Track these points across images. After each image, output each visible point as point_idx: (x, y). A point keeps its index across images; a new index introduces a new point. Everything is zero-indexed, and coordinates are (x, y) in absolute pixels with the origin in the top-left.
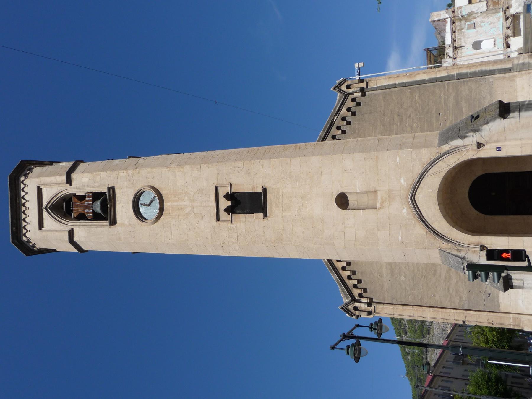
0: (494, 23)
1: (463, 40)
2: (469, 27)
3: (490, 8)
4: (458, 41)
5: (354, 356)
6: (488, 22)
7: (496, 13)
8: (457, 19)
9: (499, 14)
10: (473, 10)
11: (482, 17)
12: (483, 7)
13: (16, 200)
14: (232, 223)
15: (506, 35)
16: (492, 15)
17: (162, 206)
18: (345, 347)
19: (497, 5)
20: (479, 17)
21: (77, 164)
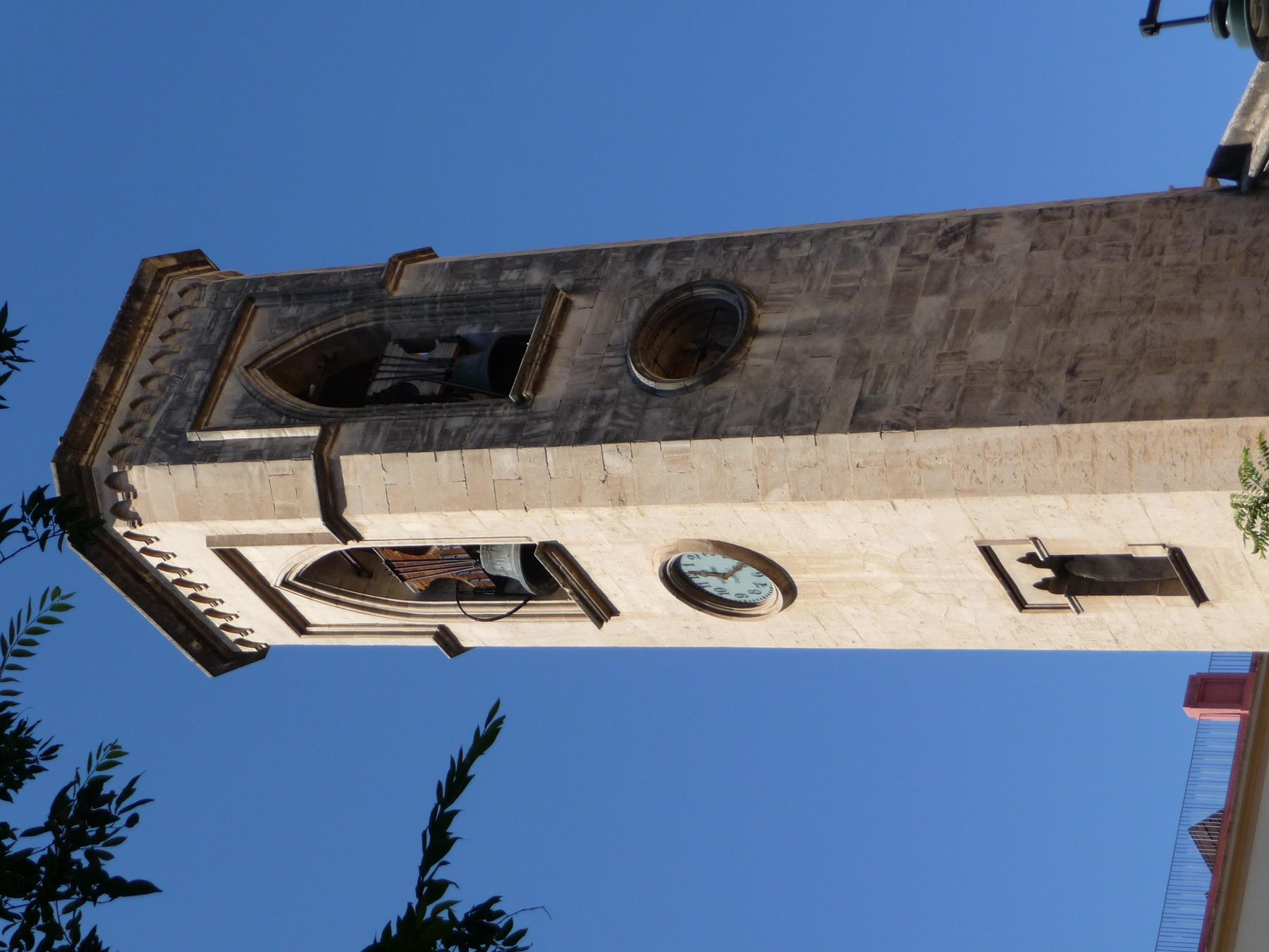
13: (141, 580)
14: (1078, 612)
17: (785, 584)
21: (327, 466)
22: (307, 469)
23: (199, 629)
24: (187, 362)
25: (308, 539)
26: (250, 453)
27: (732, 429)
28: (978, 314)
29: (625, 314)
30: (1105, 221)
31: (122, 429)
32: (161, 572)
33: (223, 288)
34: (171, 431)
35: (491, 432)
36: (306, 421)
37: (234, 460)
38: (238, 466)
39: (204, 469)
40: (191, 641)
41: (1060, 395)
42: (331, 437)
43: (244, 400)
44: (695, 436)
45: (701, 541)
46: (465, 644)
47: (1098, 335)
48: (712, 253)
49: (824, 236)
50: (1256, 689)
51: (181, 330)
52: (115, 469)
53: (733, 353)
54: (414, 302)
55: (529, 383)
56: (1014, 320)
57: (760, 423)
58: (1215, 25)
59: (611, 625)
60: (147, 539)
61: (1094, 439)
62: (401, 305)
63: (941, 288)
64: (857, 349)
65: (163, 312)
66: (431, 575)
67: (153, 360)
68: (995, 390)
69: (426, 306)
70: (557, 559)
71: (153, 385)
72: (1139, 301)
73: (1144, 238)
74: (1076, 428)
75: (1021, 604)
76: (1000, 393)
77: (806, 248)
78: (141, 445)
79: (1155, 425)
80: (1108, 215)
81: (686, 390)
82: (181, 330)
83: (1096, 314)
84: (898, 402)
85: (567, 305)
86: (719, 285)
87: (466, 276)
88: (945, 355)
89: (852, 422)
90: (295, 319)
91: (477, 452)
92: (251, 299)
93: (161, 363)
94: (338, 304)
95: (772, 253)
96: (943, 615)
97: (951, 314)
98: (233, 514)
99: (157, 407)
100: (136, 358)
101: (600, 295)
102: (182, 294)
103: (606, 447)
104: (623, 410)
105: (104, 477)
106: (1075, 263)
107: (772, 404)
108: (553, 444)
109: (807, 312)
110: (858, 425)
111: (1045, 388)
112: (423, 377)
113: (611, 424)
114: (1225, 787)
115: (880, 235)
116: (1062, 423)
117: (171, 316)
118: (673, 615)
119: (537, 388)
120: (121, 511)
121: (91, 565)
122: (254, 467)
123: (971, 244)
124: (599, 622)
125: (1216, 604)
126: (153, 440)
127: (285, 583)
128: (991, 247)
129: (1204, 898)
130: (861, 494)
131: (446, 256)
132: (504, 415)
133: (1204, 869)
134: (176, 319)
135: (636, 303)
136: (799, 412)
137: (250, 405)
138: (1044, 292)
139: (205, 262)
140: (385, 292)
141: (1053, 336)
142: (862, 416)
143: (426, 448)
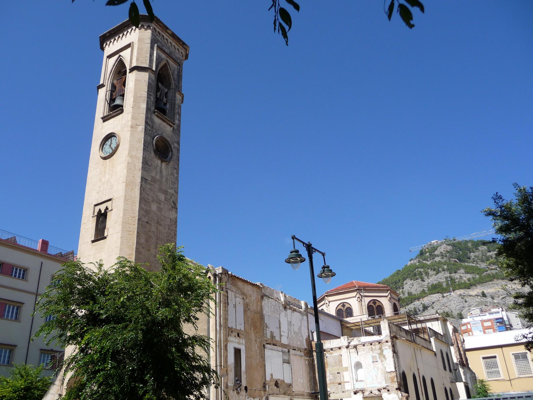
1: (363, 352)
2: (373, 357)
3: (389, 375)
4: (363, 348)
6: (377, 374)
7: (386, 380)
8: (381, 346)
9: (385, 383)
10: (387, 360)
11: (382, 368)
13: (125, 27)
15: (364, 391)
16: (384, 377)
18: (296, 248)
20: (382, 366)
22: (147, 65)
23: (111, 36)
24: (169, 49)
25: (131, 62)
26: (151, 55)
27: (144, 153)
28: (160, 206)
29: (168, 137)
31: (159, 32)
32: (127, 31)
33: (181, 61)
34: (157, 41)
35: (150, 104)
36: (156, 68)
37: (150, 52)
38: (149, 52)
39: (149, 45)
40: (109, 34)
41: (143, 219)
42: (152, 72)
45: (120, 142)
47: (153, 229)
48: (177, 157)
50: (44, 254)
51: (175, 50)
52: (151, 28)
53: (159, 156)
54: (175, 97)
55: (158, 115)
56: (158, 213)
58: (294, 250)
59: (101, 121)
61: (134, 225)
62: (175, 94)
63: (165, 200)
64: (156, 181)
66: (117, 86)
67: (170, 42)
68: (146, 207)
69: (174, 99)
70: (119, 112)
71: (166, 41)
72: (159, 238)
73: (170, 240)
75: (96, 205)
76: (145, 208)
78: (155, 35)
79: (135, 237)
80: (175, 234)
81: (153, 145)
82: (175, 50)
83: (157, 229)
84: (146, 187)
85: (171, 126)
86: (171, 157)
87: (178, 108)
88: (153, 198)
89: (143, 177)
91: (146, 100)
92: (179, 65)
94: (176, 81)
95: (175, 169)
96: (95, 189)
98: (139, 49)
101: (172, 133)
102: (181, 52)
104: (151, 132)
105: (150, 25)
108: (146, 116)
109: (164, 173)
110: (142, 178)
111: (145, 216)
112: (160, 94)
113: (148, 129)
114: (24, 245)
115: (176, 190)
116: (138, 219)
117: (178, 49)
119: (157, 116)
121: (115, 27)
122: (148, 55)
124: (102, 118)
125: (91, 245)
126: (156, 37)
128: (172, 211)
130: (127, 176)
131: (182, 105)
132: (152, 108)
134: (177, 50)
135: (170, 140)
136: (146, 167)
137: (160, 59)
138: (162, 219)
140: (178, 91)
141: (154, 220)
142: (144, 179)
143: (148, 90)
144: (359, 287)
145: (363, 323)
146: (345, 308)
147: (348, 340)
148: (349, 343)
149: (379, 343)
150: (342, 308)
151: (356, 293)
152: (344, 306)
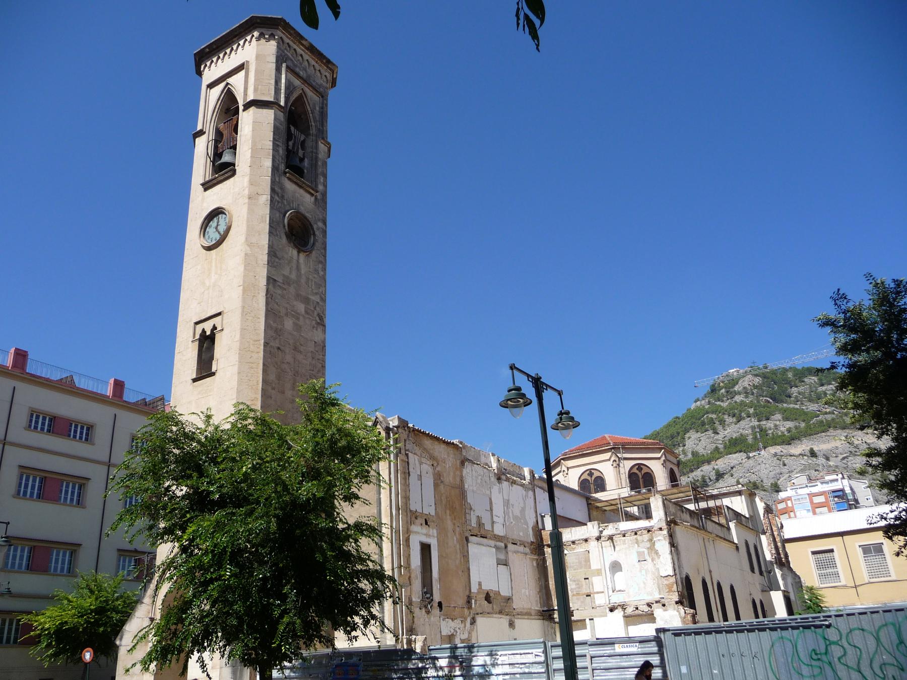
0: (645, 588)
1: (623, 546)
2: (639, 554)
5: (508, 400)
6: (646, 580)
12: (666, 570)
13: (235, 37)
16: (656, 585)
17: (212, 248)
19: (668, 590)
22: (270, 98)
24: (306, 71)
28: (298, 322)
30: (321, 365)
31: (288, 44)
35: (277, 161)
36: (286, 102)
39: (274, 66)
43: (293, 85)
44: (270, 226)
46: (197, 139)
47: (289, 358)
49: (324, 278)
52: (276, 37)
53: (294, 243)
54: (317, 147)
55: (291, 177)
57: (272, 248)
58: (512, 388)
60: (250, 42)
61: (258, 352)
63: (306, 312)
65: (321, 69)
66: (225, 133)
67: (307, 60)
70: (229, 174)
71: (300, 58)
72: (297, 372)
74: (262, 347)
75: (197, 323)
76: (274, 325)
77: (321, 273)
79: (261, 372)
81: (284, 226)
85: (312, 195)
86: (314, 244)
90: (315, 109)
91: (271, 155)
92: (322, 97)
93: (306, 63)
95: (321, 262)
97: (298, 313)
98: (257, 72)
99: (294, 57)
100: (309, 55)
101: (313, 206)
103: (269, 196)
104: (280, 204)
106: (310, 354)
107: (277, 253)
108: (271, 179)
111: (275, 339)
112: (294, 144)
117: (319, 71)
118: (202, 210)
119: (289, 179)
120: (262, 35)
122: (273, 82)
123: (318, 324)
124: (203, 185)
126: (284, 52)
127: (228, 84)
128: (317, 330)
129: (48, 377)
133: (58, 378)
135: (310, 216)
139: (332, 87)
141: (289, 344)
142: (271, 281)
144: (615, 444)
145: (622, 501)
146: (593, 478)
147: (599, 528)
148: (601, 532)
149: (649, 531)
150: (589, 478)
151: (610, 454)
152: (591, 474)
